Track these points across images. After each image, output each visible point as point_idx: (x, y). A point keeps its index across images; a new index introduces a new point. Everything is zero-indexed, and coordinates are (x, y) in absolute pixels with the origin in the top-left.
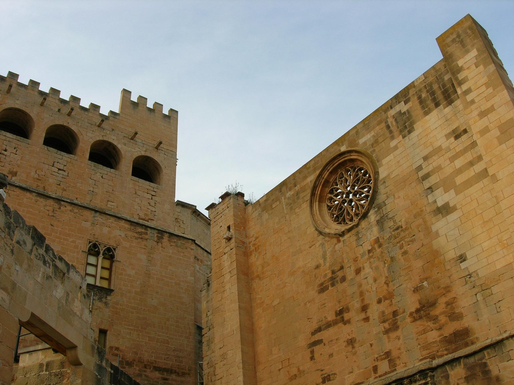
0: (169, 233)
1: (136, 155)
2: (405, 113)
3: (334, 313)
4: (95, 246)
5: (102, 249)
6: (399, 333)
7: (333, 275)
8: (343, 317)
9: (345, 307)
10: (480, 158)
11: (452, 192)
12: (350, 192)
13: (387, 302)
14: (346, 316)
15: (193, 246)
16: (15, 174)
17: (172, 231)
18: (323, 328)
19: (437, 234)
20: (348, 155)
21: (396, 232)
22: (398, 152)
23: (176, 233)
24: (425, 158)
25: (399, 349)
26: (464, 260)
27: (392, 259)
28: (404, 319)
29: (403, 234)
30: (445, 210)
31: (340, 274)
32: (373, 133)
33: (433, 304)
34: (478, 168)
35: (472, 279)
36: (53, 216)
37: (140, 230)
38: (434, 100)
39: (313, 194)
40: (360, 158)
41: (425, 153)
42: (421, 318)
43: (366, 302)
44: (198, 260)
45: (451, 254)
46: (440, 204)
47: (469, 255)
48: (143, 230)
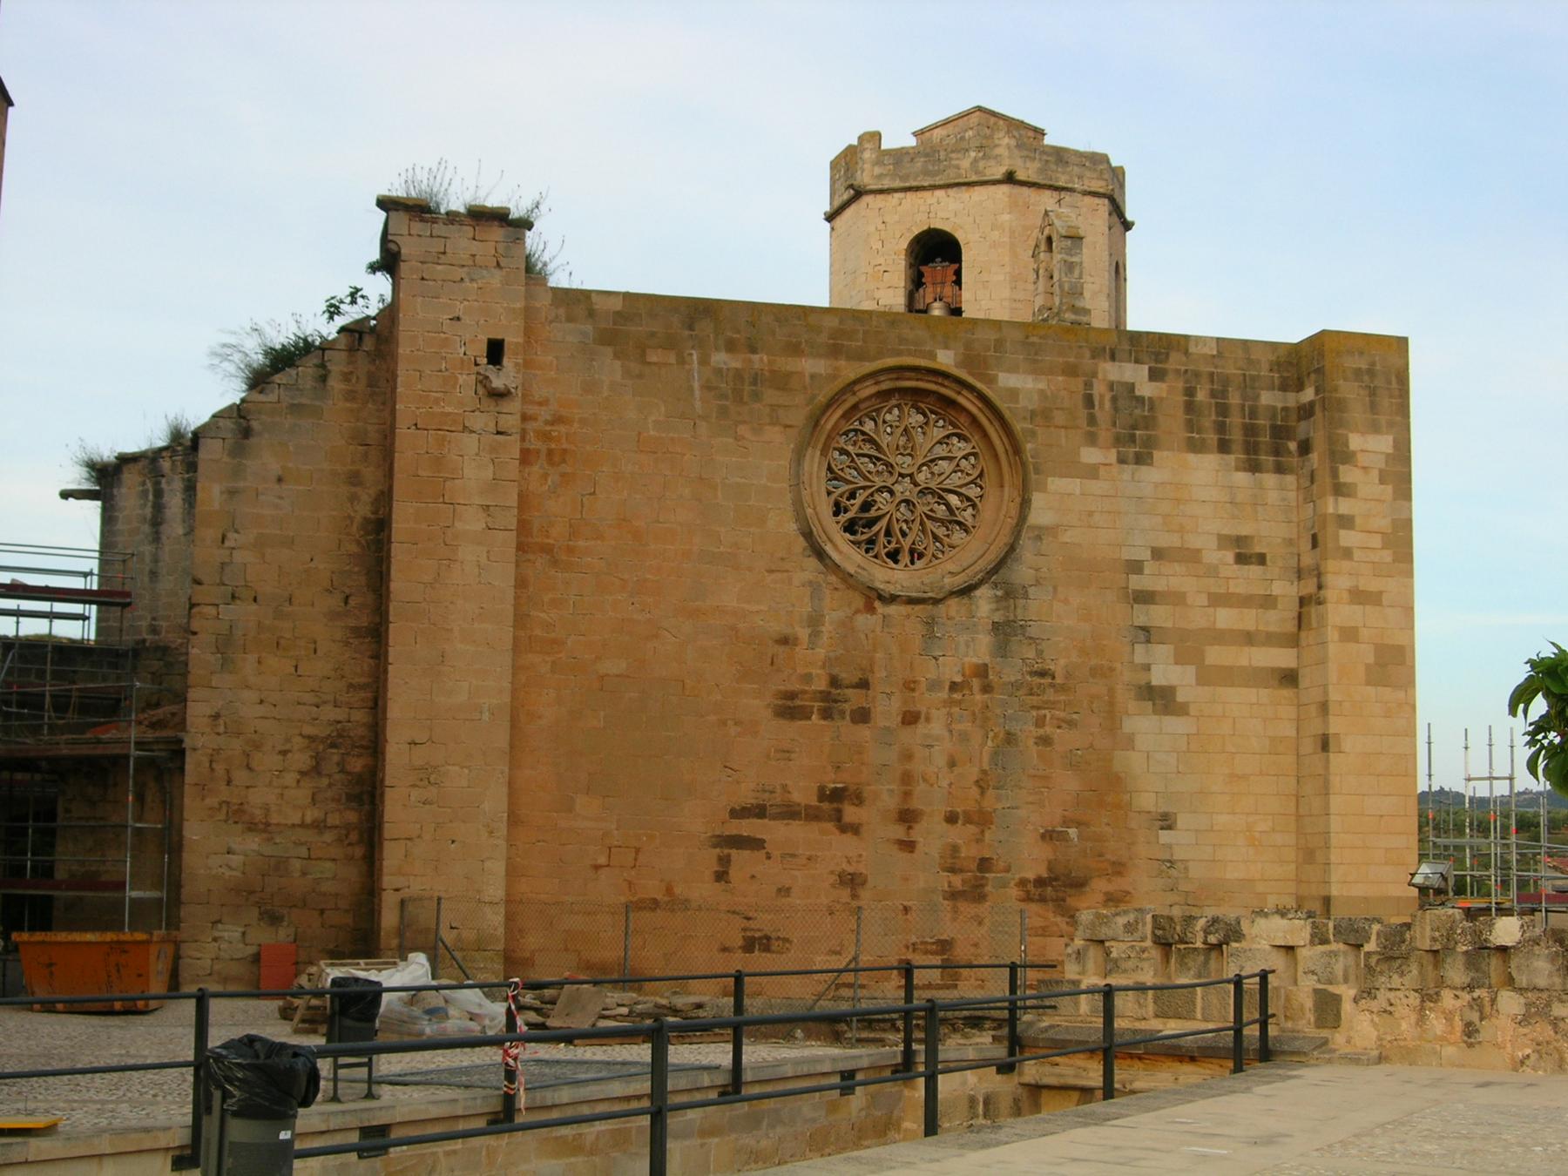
2: (1140, 400)
3: (815, 786)
6: (983, 909)
7: (834, 691)
8: (839, 812)
9: (852, 788)
11: (1191, 670)
13: (972, 829)
14: (851, 813)
18: (770, 811)
19: (1130, 743)
20: (953, 385)
21: (1037, 680)
22: (1095, 486)
24: (1158, 554)
25: (976, 945)
26: (1170, 828)
27: (1010, 739)
28: (1005, 885)
29: (1050, 695)
30: (1162, 699)
31: (855, 698)
33: (1079, 884)
35: (1173, 872)
38: (1221, 428)
41: (1167, 540)
42: (1042, 900)
43: (916, 804)
45: (1147, 801)
46: (1158, 678)
47: (1182, 821)
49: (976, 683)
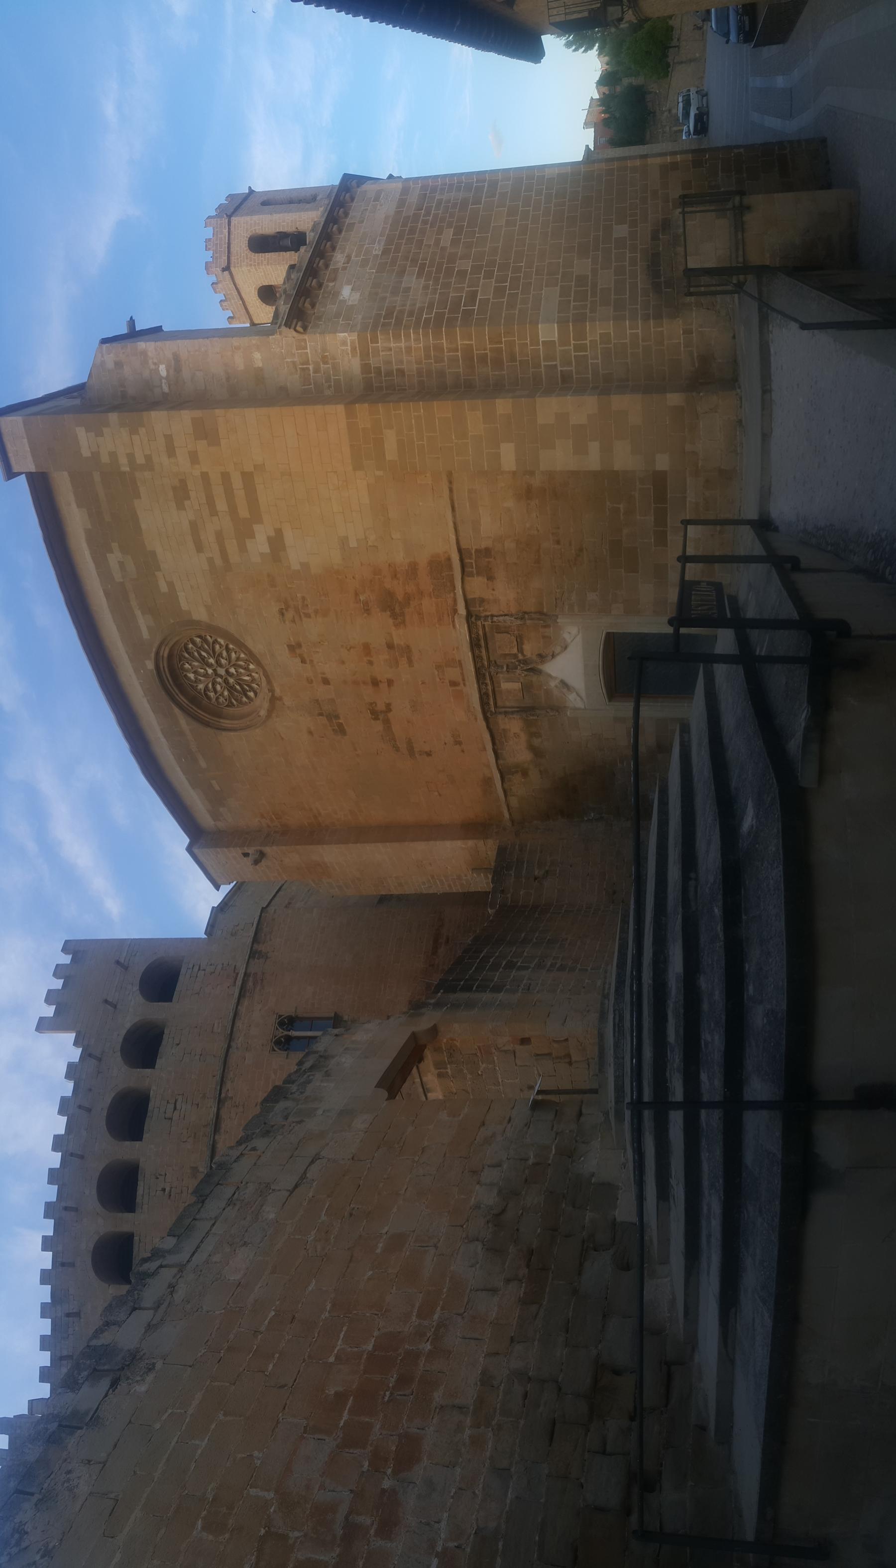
0: (253, 944)
1: (140, 999)
4: (278, 1043)
5: (281, 1033)
8: (381, 712)
10: (226, 476)
11: (256, 527)
12: (227, 672)
14: (381, 706)
15: (271, 910)
16: (195, 1170)
17: (250, 940)
19: (305, 566)
23: (252, 934)
30: (277, 543)
32: (138, 613)
33: (390, 594)
34: (237, 482)
36: (243, 1105)
37: (250, 984)
39: (207, 724)
40: (171, 644)
44: (289, 903)
46: (265, 548)
48: (251, 979)
49: (298, 651)
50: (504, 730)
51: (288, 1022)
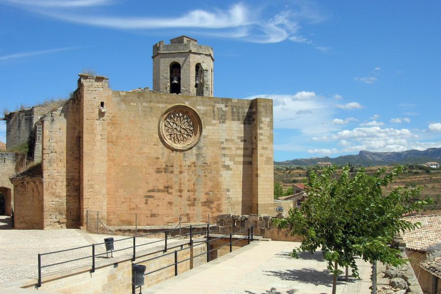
19: (221, 176)
33: (212, 202)
50: (160, 234)
51: (158, 169)
